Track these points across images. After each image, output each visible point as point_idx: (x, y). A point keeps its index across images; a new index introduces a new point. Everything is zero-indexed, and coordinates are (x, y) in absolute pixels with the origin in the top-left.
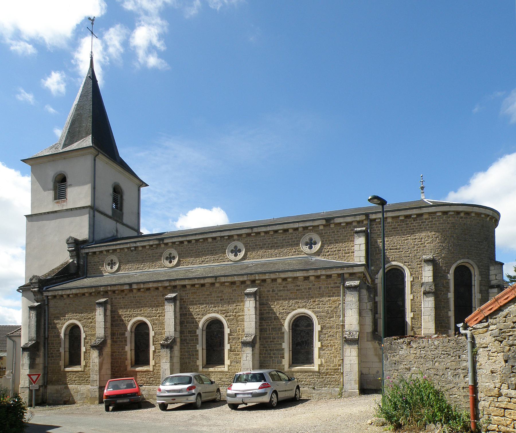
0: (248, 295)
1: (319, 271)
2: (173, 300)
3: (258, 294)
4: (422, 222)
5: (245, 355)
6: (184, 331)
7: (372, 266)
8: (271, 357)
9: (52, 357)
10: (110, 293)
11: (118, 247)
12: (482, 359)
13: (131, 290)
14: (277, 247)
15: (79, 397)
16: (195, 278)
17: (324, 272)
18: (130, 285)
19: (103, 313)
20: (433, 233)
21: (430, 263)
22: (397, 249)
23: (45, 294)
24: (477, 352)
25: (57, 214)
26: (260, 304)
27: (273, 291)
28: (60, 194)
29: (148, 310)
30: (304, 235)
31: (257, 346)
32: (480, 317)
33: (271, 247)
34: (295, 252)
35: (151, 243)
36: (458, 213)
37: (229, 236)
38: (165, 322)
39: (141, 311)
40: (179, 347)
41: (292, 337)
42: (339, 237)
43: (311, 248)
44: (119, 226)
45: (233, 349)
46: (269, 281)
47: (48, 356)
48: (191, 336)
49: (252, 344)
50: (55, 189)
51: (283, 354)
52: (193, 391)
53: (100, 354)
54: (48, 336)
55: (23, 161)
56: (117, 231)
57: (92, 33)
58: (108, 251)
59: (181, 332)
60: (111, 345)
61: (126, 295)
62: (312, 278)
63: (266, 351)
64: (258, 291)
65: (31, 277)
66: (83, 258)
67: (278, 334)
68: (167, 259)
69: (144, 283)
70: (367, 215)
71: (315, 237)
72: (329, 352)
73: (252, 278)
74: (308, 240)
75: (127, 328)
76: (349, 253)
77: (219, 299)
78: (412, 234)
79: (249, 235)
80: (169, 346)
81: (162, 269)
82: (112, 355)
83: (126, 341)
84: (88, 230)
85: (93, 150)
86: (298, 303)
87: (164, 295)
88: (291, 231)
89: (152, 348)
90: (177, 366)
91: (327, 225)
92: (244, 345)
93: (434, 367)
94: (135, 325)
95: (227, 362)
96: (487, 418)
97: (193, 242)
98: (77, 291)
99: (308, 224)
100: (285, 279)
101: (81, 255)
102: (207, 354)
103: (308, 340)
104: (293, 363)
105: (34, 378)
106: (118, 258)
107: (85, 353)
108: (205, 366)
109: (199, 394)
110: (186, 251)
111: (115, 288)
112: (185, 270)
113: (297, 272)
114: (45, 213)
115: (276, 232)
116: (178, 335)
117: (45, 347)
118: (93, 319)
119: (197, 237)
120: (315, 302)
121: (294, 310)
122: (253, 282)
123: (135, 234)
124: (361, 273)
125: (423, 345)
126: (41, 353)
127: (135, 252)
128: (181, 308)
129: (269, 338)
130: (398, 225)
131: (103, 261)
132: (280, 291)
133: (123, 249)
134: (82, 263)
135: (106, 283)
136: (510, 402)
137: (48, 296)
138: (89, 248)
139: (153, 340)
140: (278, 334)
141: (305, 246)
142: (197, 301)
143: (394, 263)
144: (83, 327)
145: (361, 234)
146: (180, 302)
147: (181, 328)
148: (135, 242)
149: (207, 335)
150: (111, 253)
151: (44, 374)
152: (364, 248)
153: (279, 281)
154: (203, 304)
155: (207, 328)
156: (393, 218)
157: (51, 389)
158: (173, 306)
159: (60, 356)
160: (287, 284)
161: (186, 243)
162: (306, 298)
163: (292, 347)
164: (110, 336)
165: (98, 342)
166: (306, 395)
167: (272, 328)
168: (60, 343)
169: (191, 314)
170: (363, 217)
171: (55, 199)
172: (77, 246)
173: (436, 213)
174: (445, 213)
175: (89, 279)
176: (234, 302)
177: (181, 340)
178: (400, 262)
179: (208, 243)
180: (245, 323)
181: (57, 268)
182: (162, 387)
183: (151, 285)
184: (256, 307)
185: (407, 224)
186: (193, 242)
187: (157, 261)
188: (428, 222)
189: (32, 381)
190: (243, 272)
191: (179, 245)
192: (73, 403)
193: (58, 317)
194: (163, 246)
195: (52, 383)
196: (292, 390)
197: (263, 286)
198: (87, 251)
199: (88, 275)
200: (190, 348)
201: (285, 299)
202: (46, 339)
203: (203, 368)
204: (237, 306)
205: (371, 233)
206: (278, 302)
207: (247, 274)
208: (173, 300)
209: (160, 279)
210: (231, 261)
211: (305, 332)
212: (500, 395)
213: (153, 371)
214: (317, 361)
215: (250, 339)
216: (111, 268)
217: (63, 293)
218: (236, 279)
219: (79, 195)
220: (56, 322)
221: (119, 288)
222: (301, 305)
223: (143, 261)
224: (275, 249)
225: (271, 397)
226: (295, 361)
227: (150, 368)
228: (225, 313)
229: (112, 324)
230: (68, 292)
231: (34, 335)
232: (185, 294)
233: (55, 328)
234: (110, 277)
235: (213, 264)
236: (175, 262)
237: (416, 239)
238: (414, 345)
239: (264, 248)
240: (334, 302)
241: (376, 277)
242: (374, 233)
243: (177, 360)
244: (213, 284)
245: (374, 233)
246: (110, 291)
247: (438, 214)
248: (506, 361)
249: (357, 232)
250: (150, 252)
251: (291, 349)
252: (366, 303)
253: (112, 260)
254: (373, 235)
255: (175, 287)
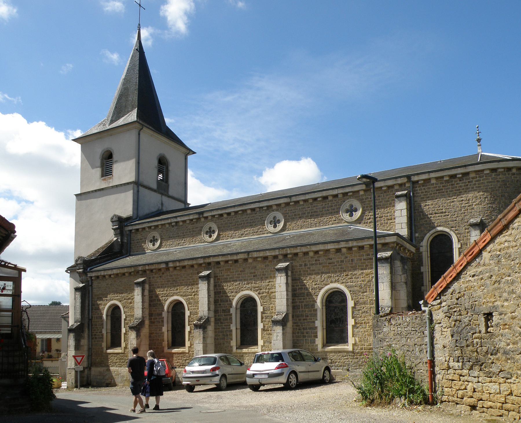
0: (279, 270)
1: (350, 242)
2: (207, 278)
3: (290, 269)
4: (469, 182)
5: (275, 334)
6: (218, 311)
7: (416, 232)
8: (304, 336)
9: (96, 338)
10: (148, 272)
11: (159, 223)
12: (437, 335)
13: (168, 269)
14: (317, 216)
15: (120, 379)
16: (228, 254)
17: (355, 244)
18: (167, 263)
19: (141, 294)
20: (481, 193)
21: (477, 227)
22: (442, 213)
23: (89, 275)
24: (434, 327)
25: (104, 191)
26: (292, 280)
27: (305, 265)
28: (106, 171)
29: (184, 289)
30: (344, 201)
31: (290, 324)
32: (435, 295)
33: (311, 216)
34: (335, 220)
35: (191, 217)
36: (509, 169)
37: (267, 206)
38: (199, 301)
39: (177, 290)
40: (213, 327)
41: (326, 314)
42: (380, 202)
43: (351, 215)
44: (165, 199)
45: (266, 328)
46: (301, 255)
47: (92, 337)
48: (225, 315)
49: (283, 323)
50: (102, 166)
51: (316, 333)
52: (217, 372)
53: (138, 336)
54: (92, 317)
55: (74, 140)
56: (162, 204)
57: (140, 5)
58: (150, 227)
59: (216, 312)
60: (149, 326)
61: (163, 274)
62: (344, 250)
63: (299, 330)
64: (290, 266)
65: (77, 258)
66: (127, 235)
67: (311, 311)
68: (207, 233)
69: (179, 261)
70: (409, 177)
71: (356, 203)
72: (363, 330)
73: (284, 252)
74: (348, 207)
75: (164, 308)
76: (391, 219)
77: (252, 275)
78: (458, 195)
79: (287, 204)
80: (202, 326)
81: (202, 245)
82: (150, 337)
83: (163, 321)
84: (132, 206)
85: (137, 125)
86: (331, 277)
87: (198, 273)
88: (330, 198)
89: (187, 329)
90: (211, 347)
91: (368, 190)
92: (274, 324)
93: (407, 343)
94: (172, 305)
95: (260, 342)
96: (441, 390)
97: (233, 214)
98: (118, 271)
99: (347, 190)
100: (316, 252)
101: (124, 233)
102: (241, 334)
103: (342, 317)
104: (327, 342)
105: (79, 359)
106: (160, 234)
107: (125, 334)
108: (239, 347)
109: (224, 376)
110: (226, 224)
111: (153, 267)
112: (223, 245)
113: (329, 245)
114: (92, 191)
115: (315, 199)
116: (212, 314)
117: (89, 328)
118: (132, 299)
119: (237, 209)
120: (347, 275)
121: (326, 285)
122: (285, 256)
123: (182, 206)
124: (394, 243)
125: (399, 322)
126: (86, 335)
127: (176, 227)
128: (215, 286)
129: (302, 315)
130: (443, 186)
131: (146, 238)
132: (312, 264)
133: (164, 224)
134: (126, 241)
135: (144, 262)
136: (455, 374)
137: (91, 277)
138: (132, 225)
139: (189, 319)
140: (311, 311)
141: (346, 214)
142: (232, 278)
143: (439, 229)
144: (124, 307)
145: (402, 198)
146: (214, 280)
147: (215, 307)
148: (176, 217)
149: (241, 314)
150: (153, 229)
151: (89, 356)
152: (406, 214)
153: (311, 254)
154: (237, 281)
155: (241, 306)
156: (437, 178)
157: (95, 371)
158: (207, 284)
159: (102, 338)
160: (319, 257)
161: (225, 216)
162: (339, 271)
163: (327, 325)
164: (148, 317)
165: (136, 322)
166: (340, 377)
167: (305, 305)
168: (103, 324)
169: (225, 293)
170: (405, 180)
171: (102, 176)
172: (121, 223)
173: (483, 171)
174: (494, 170)
175: (131, 257)
176: (267, 278)
177: (216, 319)
178: (446, 227)
179: (247, 214)
180: (277, 301)
181: (102, 248)
182: (188, 368)
183: (186, 263)
184: (287, 283)
185: (452, 185)
186: (233, 214)
187: (197, 236)
188: (475, 181)
189: (77, 363)
190: (275, 246)
191: (218, 218)
192: (115, 385)
193: (101, 298)
194: (203, 220)
195: (97, 365)
196: (318, 371)
197: (295, 260)
198: (130, 228)
199: (132, 253)
200: (224, 328)
201: (317, 274)
202: (90, 320)
203: (237, 349)
204: (270, 282)
205: (414, 196)
206: (310, 276)
207: (278, 249)
208: (207, 278)
209: (195, 256)
210: (271, 233)
211: (339, 308)
212: (449, 368)
213: (188, 353)
214: (351, 340)
215: (280, 317)
216: (154, 245)
217: (105, 274)
218: (268, 254)
219: (124, 171)
220: (99, 302)
221: (156, 266)
222: (334, 280)
223: (183, 236)
224: (315, 218)
225: (289, 378)
226: (329, 340)
227: (186, 350)
228: (258, 290)
229: (150, 305)
230: (110, 272)
231: (79, 316)
232: (218, 270)
233: (98, 309)
234: (151, 255)
235: (252, 237)
236: (215, 236)
237: (462, 200)
238: (393, 322)
239: (303, 217)
240: (367, 275)
241: (421, 245)
242: (417, 196)
243: (210, 341)
244: (246, 260)
245: (417, 196)
246: (148, 270)
247: (486, 172)
248: (452, 336)
249: (398, 197)
250: (190, 227)
251: (325, 327)
252: (400, 275)
253: (154, 237)
254: (416, 199)
255: (209, 264)
